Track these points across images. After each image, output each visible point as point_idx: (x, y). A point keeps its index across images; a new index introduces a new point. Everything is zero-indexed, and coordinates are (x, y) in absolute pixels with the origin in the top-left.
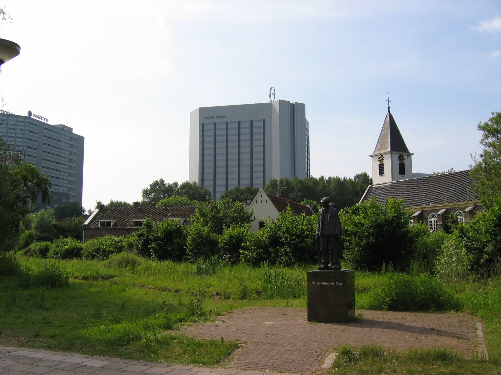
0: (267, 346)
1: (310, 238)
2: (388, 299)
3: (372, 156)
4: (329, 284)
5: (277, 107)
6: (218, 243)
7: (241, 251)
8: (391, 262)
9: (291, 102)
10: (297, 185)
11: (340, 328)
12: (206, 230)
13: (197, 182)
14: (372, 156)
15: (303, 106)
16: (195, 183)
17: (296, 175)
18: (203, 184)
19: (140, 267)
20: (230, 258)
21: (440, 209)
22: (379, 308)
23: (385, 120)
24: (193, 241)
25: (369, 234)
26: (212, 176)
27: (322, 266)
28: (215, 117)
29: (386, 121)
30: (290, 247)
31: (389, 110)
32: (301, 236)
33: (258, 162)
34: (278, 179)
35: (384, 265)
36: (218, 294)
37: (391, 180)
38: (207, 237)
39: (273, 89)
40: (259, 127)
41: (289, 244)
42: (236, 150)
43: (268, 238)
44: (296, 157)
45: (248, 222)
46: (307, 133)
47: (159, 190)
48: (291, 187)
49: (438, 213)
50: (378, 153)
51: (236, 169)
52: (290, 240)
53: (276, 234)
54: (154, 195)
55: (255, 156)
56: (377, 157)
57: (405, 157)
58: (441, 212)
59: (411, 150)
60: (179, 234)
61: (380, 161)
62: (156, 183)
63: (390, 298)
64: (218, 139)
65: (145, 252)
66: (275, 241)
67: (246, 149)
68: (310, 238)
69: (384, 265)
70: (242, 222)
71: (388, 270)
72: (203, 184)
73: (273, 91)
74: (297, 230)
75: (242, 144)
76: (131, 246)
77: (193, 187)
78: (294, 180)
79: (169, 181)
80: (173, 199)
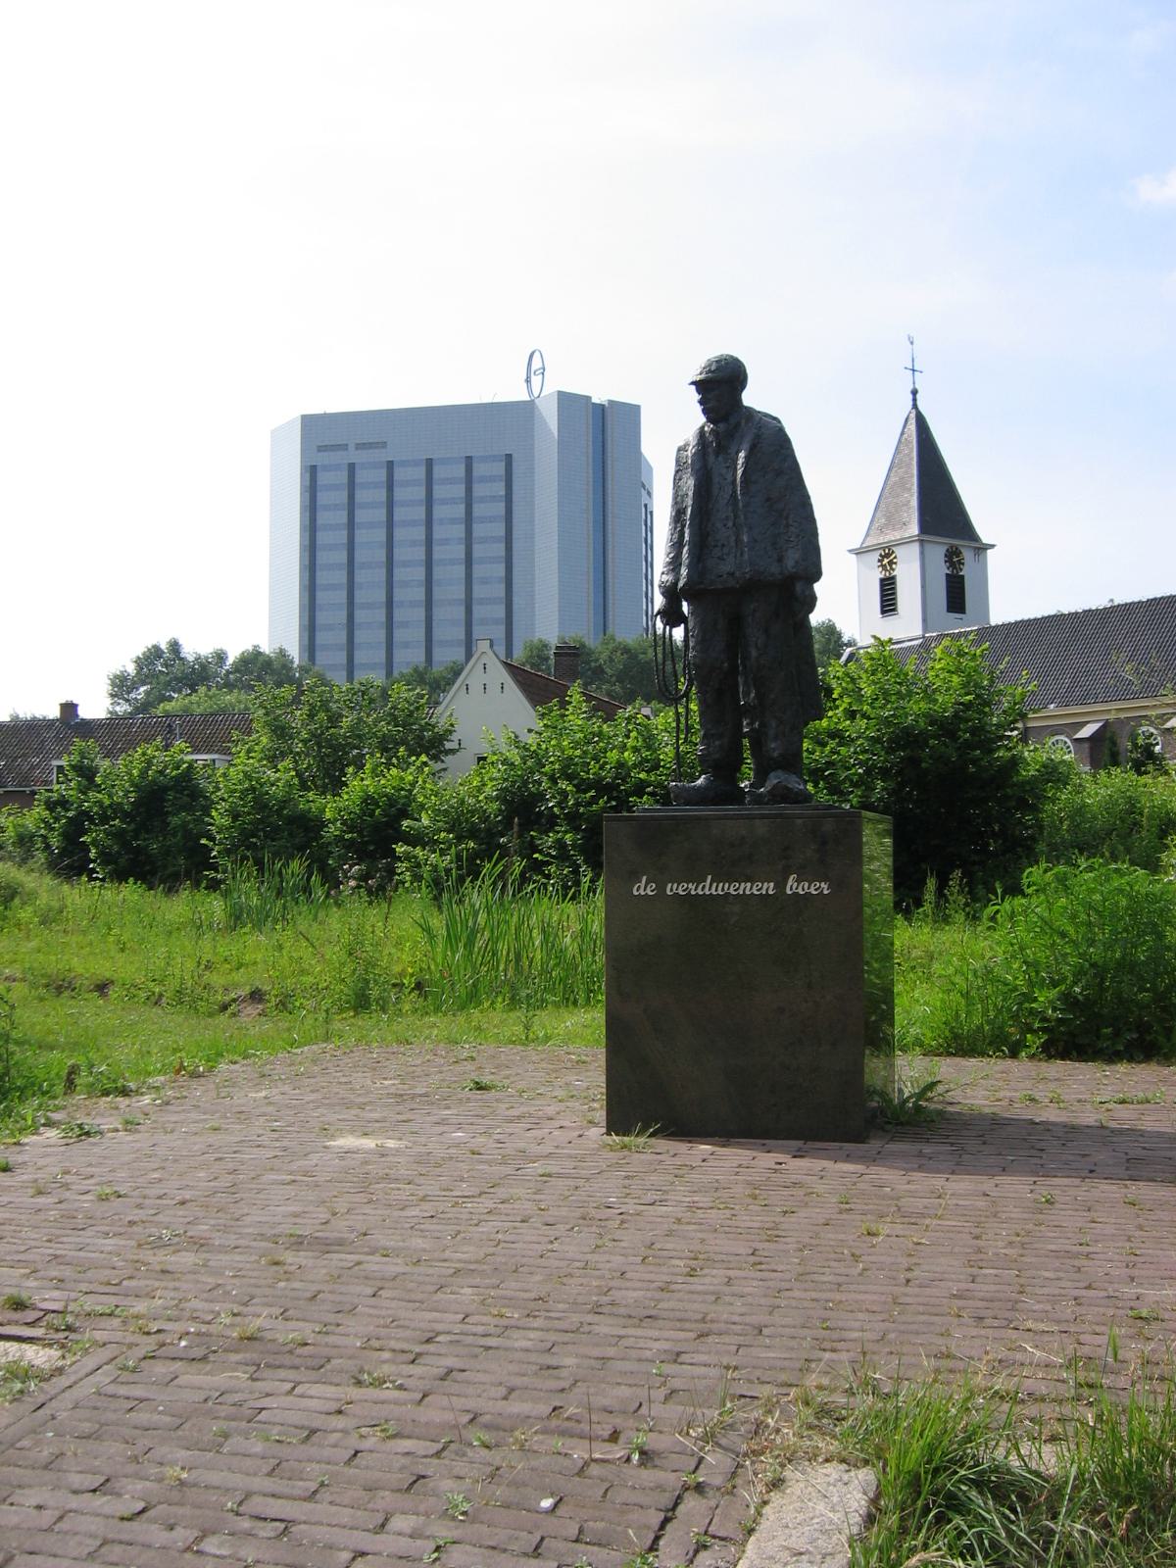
0: (221, 1380)
1: (649, 794)
2: (1044, 997)
3: (858, 552)
4: (746, 888)
5: (550, 415)
6: (323, 824)
7: (400, 849)
8: (958, 873)
9: (595, 400)
10: (611, 660)
11: (822, 1178)
12: (279, 780)
13: (294, 652)
14: (858, 552)
15: (631, 413)
16: (282, 653)
17: (610, 631)
18: (312, 658)
19: (30, 909)
20: (364, 878)
21: (1083, 724)
22: (998, 1042)
23: (902, 433)
24: (235, 816)
25: (868, 772)
26: (343, 638)
27: (700, 781)
28: (352, 447)
29: (905, 436)
30: (576, 829)
31: (915, 400)
32: (616, 790)
33: (488, 589)
34: (553, 641)
35: (931, 884)
36: (256, 996)
37: (919, 632)
38: (285, 803)
39: (537, 357)
40: (492, 479)
41: (573, 819)
42: (420, 553)
43: (497, 798)
44: (610, 556)
45: (436, 758)
46: (645, 499)
47: (164, 672)
48: (593, 664)
49: (1077, 736)
50: (875, 542)
51: (420, 613)
52: (577, 804)
53: (525, 783)
54: (147, 693)
55: (478, 571)
56: (876, 556)
57: (967, 555)
58: (1086, 732)
59: (984, 534)
60: (188, 795)
61: (884, 567)
62: (155, 653)
63: (1053, 993)
64: (361, 516)
65: (71, 863)
66: (522, 808)
67: (448, 550)
68: (649, 794)
69: (931, 884)
70: (412, 752)
71: (947, 901)
72: (312, 658)
73: (536, 364)
74: (602, 768)
75: (438, 533)
76: (25, 841)
77: (276, 666)
78: (605, 643)
79: (195, 647)
80: (200, 701)
